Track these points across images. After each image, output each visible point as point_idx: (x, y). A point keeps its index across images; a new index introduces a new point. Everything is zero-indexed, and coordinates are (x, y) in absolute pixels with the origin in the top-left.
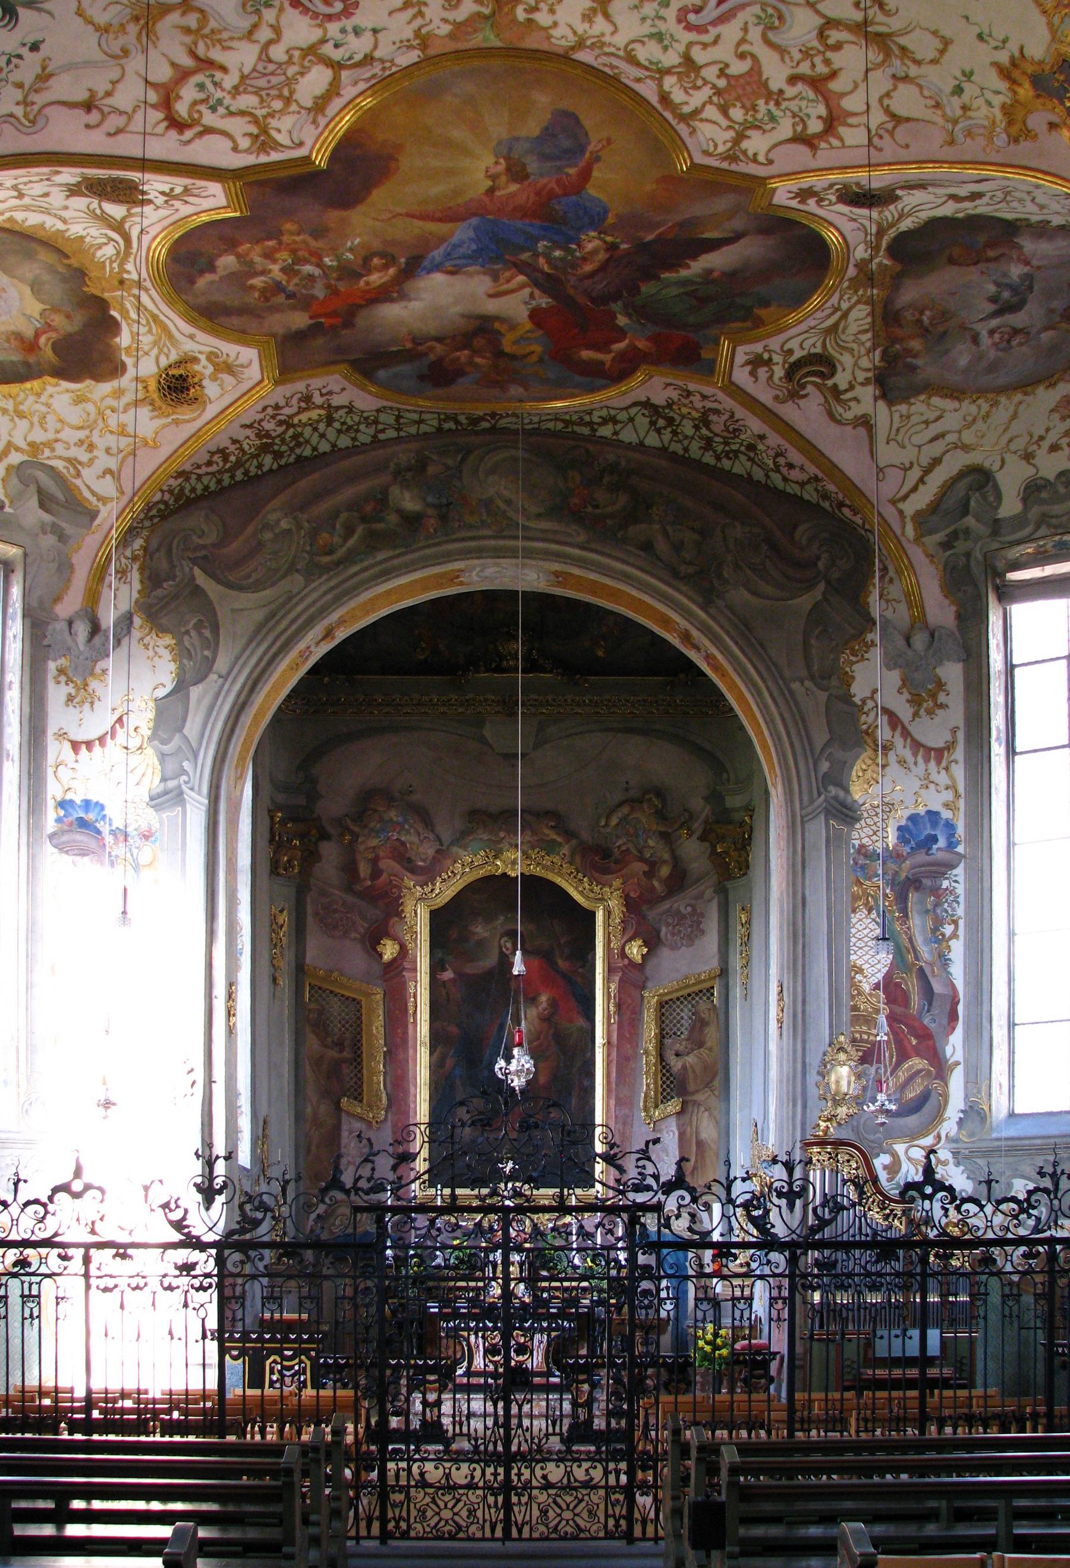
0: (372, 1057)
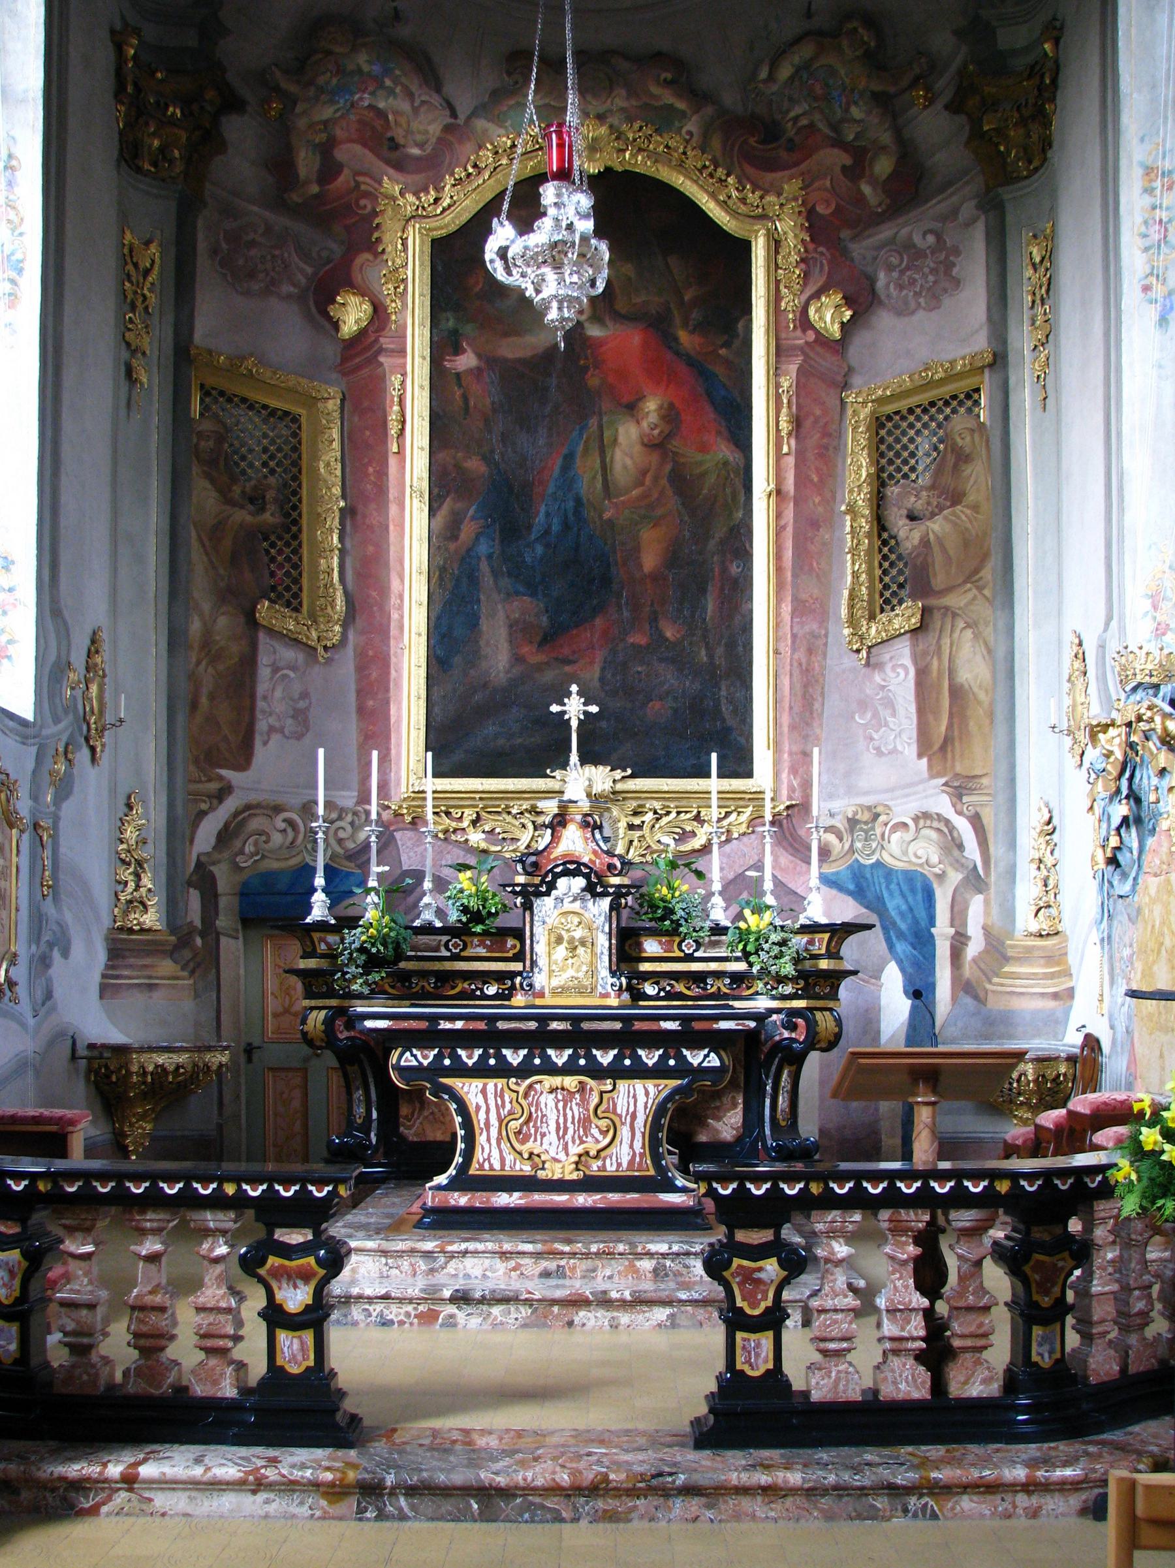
0: (318, 519)
